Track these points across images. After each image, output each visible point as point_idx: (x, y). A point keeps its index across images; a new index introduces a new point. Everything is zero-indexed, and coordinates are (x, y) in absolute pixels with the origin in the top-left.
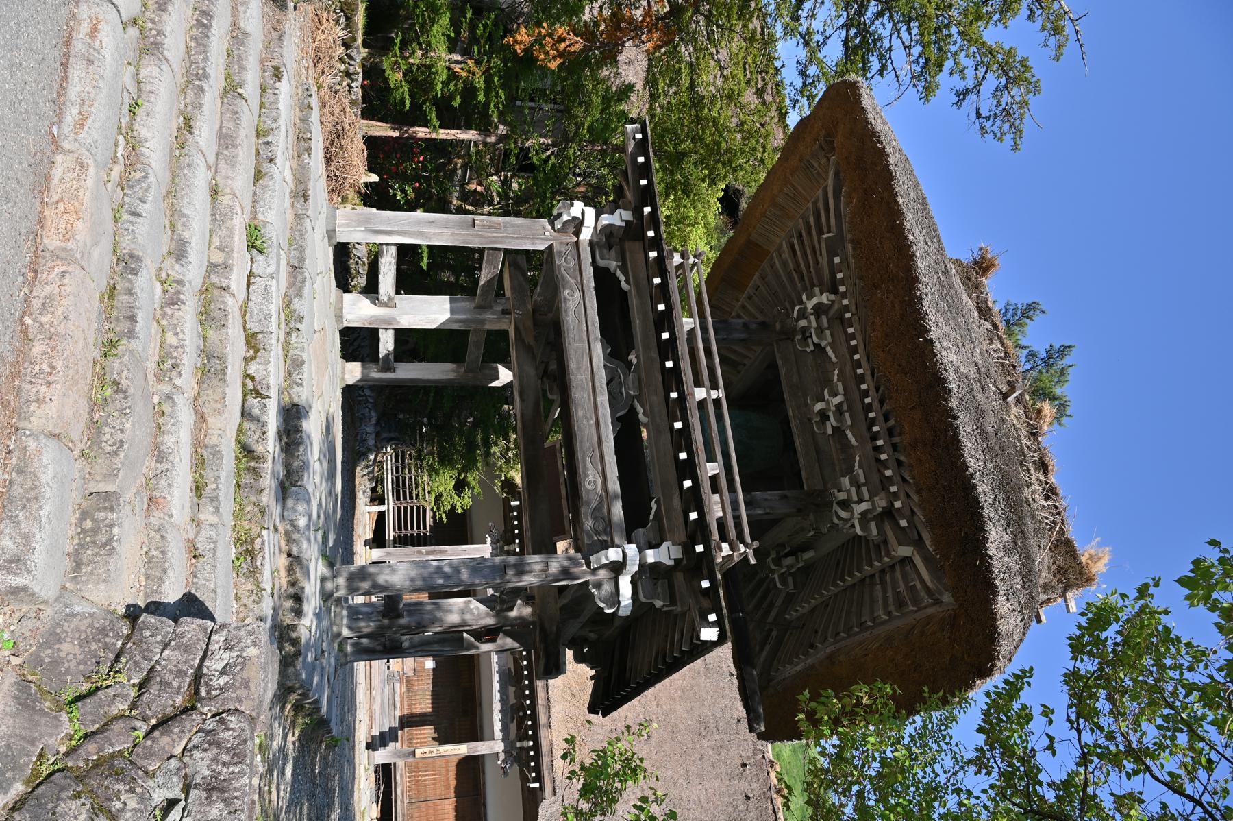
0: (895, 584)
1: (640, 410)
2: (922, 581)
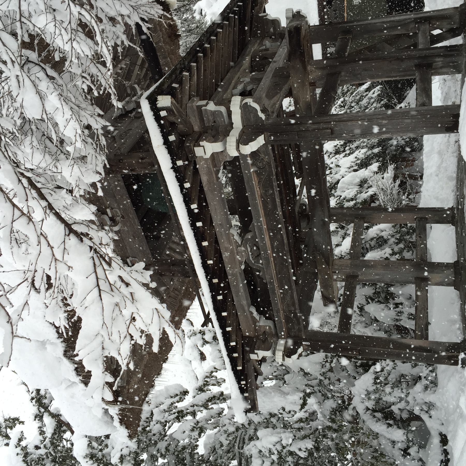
1: (237, 238)
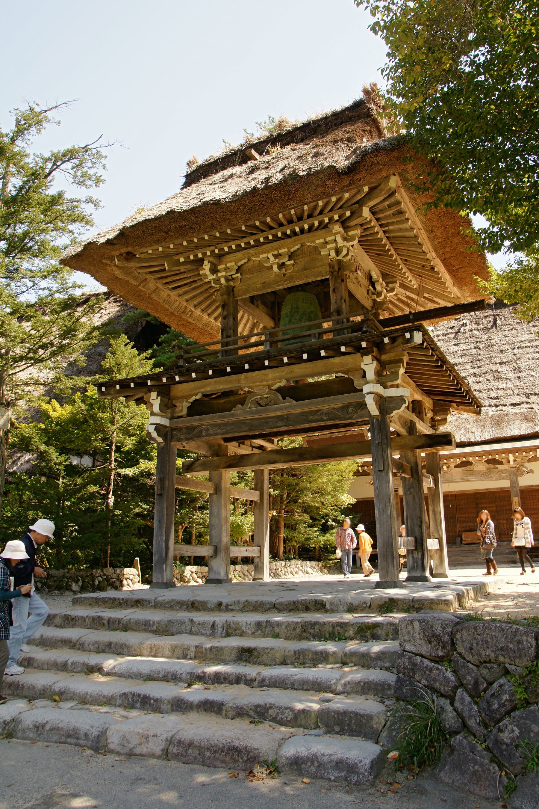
0: (386, 217)
1: (277, 385)
2: (381, 202)
